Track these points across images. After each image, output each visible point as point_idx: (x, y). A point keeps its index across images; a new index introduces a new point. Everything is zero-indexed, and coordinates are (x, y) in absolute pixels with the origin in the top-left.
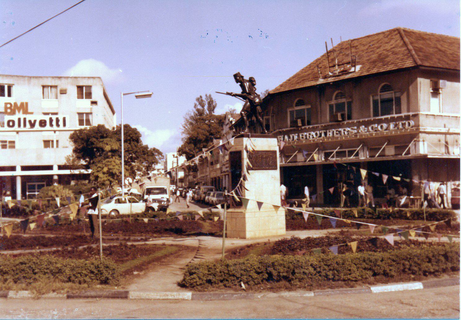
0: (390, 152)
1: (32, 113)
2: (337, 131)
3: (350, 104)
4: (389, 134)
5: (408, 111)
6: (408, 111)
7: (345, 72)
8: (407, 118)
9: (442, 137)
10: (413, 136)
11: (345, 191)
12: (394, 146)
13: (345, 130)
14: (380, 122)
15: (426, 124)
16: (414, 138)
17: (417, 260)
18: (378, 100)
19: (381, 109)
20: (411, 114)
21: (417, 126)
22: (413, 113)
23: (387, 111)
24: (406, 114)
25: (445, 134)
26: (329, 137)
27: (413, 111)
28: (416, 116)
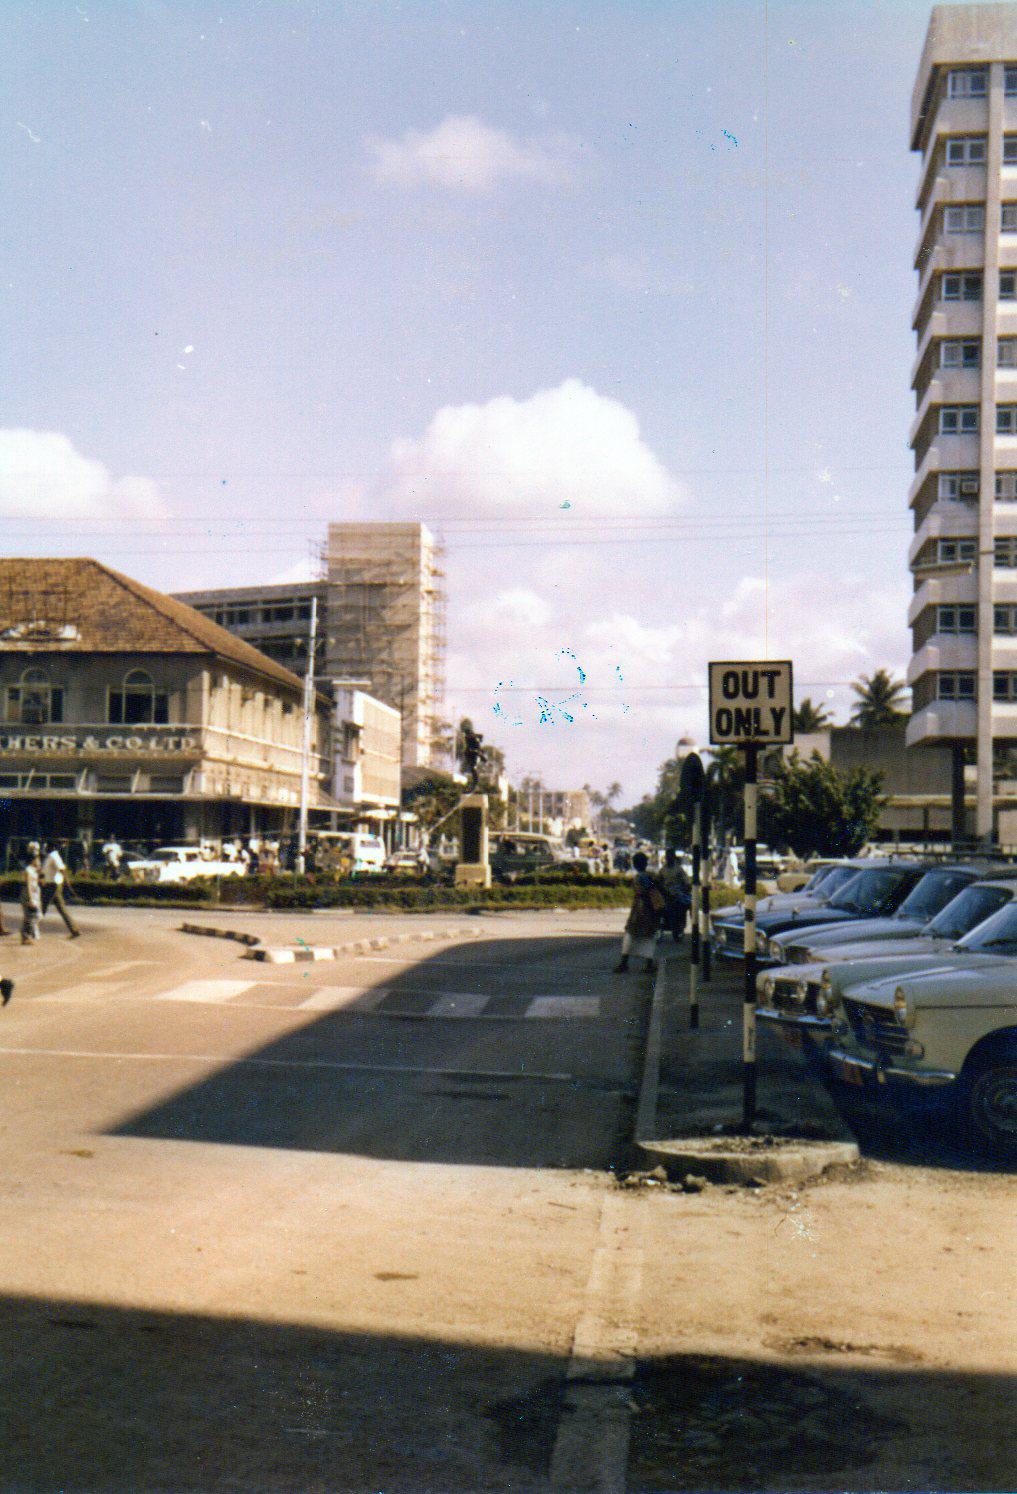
0: (139, 788)
1: (211, 695)
2: (32, 740)
3: (57, 695)
4: (146, 756)
5: (183, 719)
6: (183, 719)
7: (45, 635)
8: (181, 732)
9: (223, 767)
10: (191, 765)
11: (876, 1077)
12: (149, 776)
13: (51, 740)
14: (126, 733)
15: (213, 747)
16: (192, 766)
17: (788, 1183)
18: (121, 695)
19: (121, 706)
20: (188, 726)
21: (199, 747)
22: (193, 726)
23: (135, 716)
24: (180, 725)
25: (229, 764)
26: (12, 750)
27: (192, 722)
28: (197, 732)
